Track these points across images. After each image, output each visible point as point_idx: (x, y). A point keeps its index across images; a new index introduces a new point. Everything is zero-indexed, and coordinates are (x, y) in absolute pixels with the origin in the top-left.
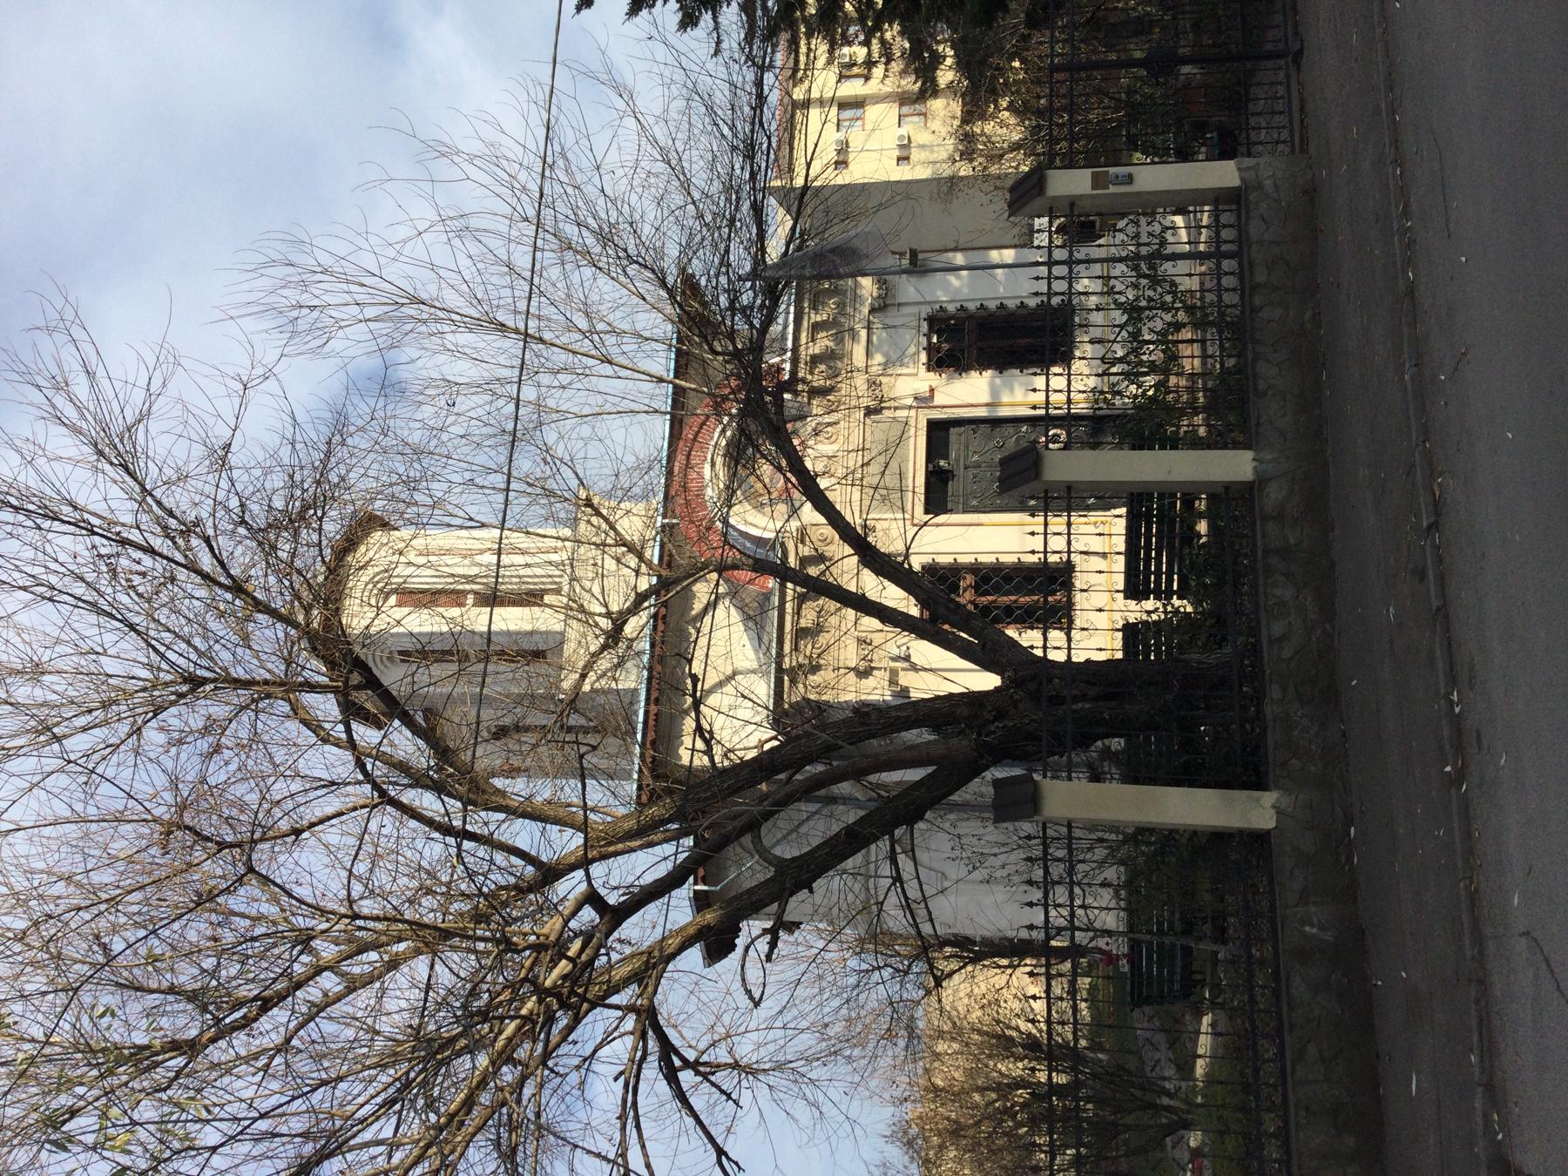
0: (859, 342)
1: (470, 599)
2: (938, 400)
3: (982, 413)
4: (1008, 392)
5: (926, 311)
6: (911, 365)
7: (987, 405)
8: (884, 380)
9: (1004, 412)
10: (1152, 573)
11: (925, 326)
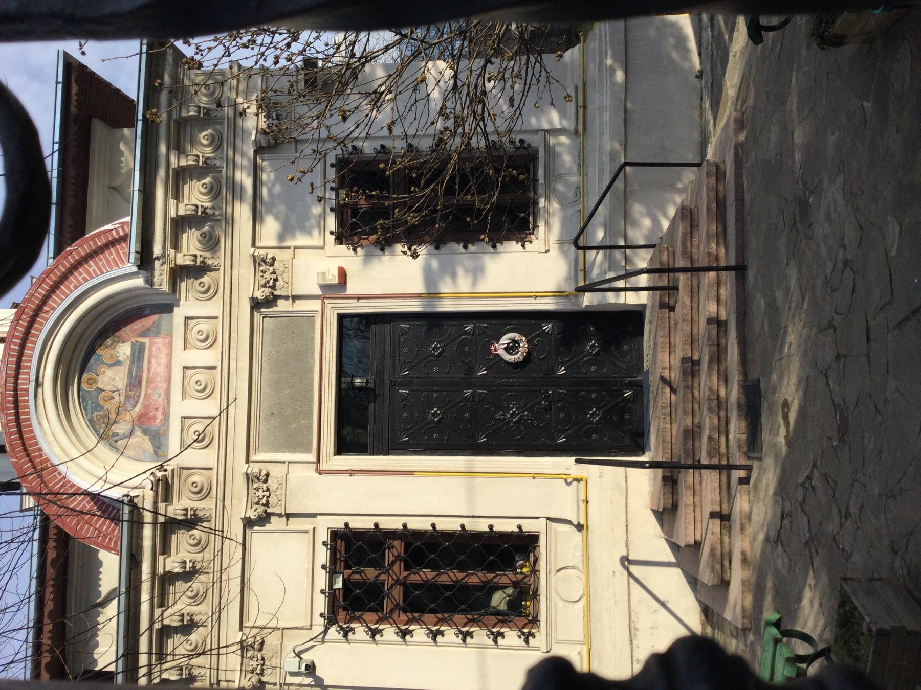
2: (351, 289)
3: (414, 306)
4: (448, 280)
6: (316, 233)
7: (419, 296)
8: (280, 255)
9: (447, 306)
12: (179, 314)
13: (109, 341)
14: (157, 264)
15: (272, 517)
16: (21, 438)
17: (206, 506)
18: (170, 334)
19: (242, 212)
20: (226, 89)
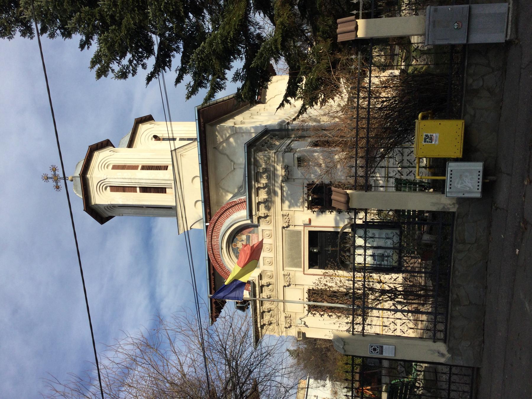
0: (278, 196)
1: (138, 189)
2: (312, 224)
3: (332, 230)
5: (306, 182)
7: (333, 227)
10: (409, 390)
11: (306, 190)
12: (260, 229)
13: (239, 234)
14: (254, 217)
15: (461, 157)
16: (215, 258)
17: (272, 281)
18: (258, 233)
19: (278, 200)
20: (271, 161)
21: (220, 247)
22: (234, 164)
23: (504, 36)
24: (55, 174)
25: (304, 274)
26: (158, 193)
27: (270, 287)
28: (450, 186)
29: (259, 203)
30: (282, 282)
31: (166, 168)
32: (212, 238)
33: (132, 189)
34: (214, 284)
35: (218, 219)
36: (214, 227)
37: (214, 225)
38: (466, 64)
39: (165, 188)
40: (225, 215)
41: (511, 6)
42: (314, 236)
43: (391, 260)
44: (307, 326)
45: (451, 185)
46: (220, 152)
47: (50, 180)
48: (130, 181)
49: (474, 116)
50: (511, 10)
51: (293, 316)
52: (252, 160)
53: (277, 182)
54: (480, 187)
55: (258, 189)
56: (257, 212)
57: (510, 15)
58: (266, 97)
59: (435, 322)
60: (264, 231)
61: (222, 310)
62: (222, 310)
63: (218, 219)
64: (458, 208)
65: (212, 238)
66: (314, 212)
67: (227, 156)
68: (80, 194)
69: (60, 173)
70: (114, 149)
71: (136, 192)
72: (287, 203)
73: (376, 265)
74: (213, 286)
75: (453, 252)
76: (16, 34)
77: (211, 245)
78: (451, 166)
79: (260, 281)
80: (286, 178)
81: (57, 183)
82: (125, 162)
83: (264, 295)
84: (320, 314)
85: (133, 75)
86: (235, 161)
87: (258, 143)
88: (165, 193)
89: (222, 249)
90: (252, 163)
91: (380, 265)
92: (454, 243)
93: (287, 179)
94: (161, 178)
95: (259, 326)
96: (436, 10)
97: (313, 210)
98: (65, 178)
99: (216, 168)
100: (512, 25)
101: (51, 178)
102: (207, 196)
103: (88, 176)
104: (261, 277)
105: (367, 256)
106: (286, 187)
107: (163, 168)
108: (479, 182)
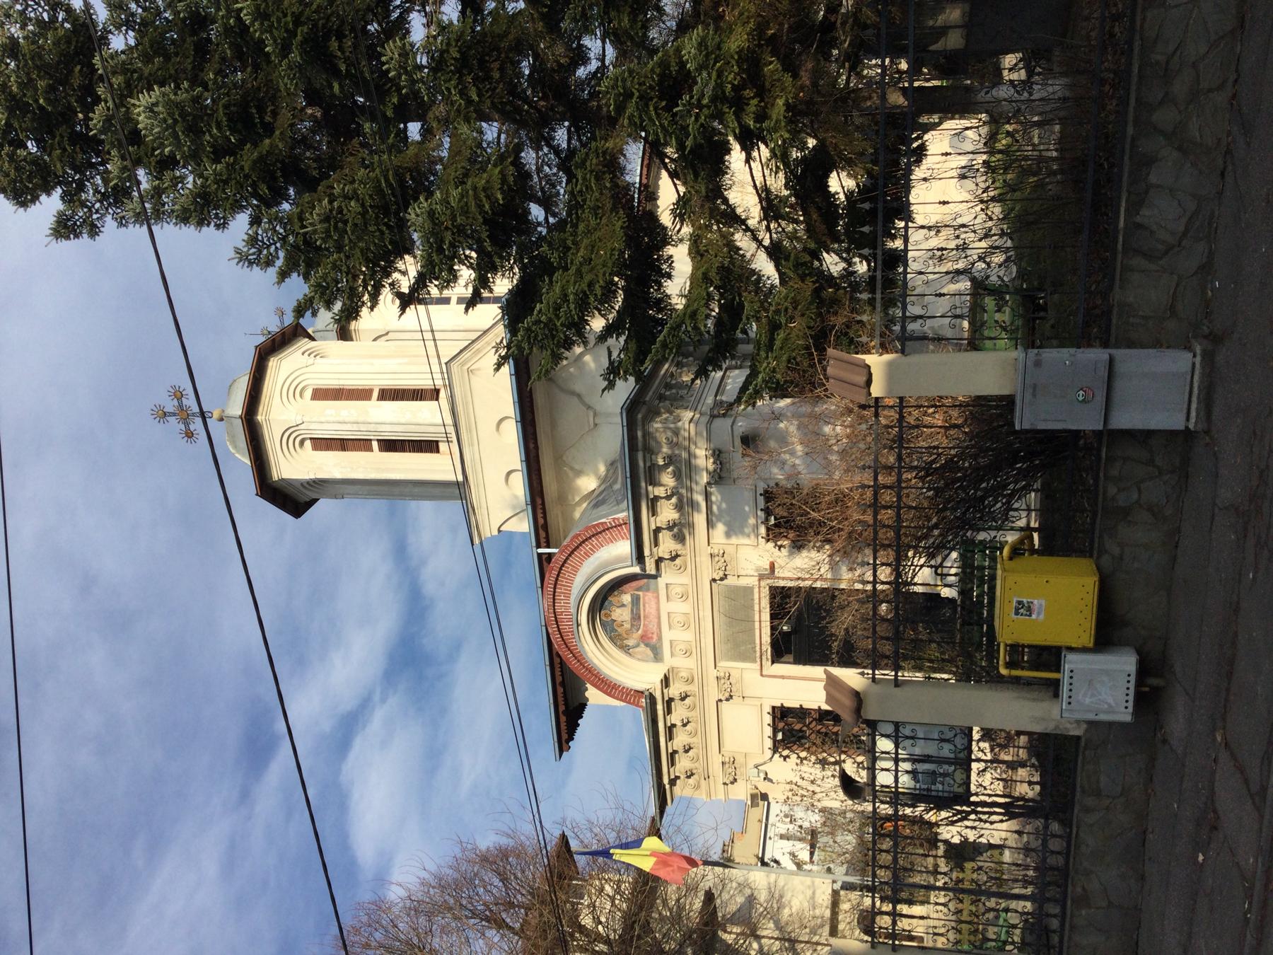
5: (761, 487)
12: (661, 582)
13: (616, 593)
14: (647, 559)
18: (657, 591)
19: (700, 519)
20: (681, 439)
21: (574, 620)
22: (595, 415)
23: (1182, 417)
24: (181, 406)
25: (762, 675)
26: (422, 452)
27: (687, 701)
28: (1070, 694)
29: (657, 531)
30: (713, 693)
31: (434, 394)
32: (554, 599)
33: (362, 444)
34: (562, 675)
35: (567, 558)
36: (558, 575)
37: (559, 572)
38: (1104, 455)
39: (437, 442)
40: (582, 550)
41: (1198, 359)
42: (781, 598)
43: (952, 782)
44: (771, 781)
45: (1070, 697)
46: (563, 390)
47: (172, 419)
48: (355, 427)
49: (1121, 558)
50: (1198, 366)
51: (740, 760)
52: (639, 434)
53: (697, 483)
54: (1130, 704)
55: (657, 531)
56: (655, 550)
57: (1196, 378)
58: (659, 202)
59: (1045, 835)
60: (671, 588)
61: (579, 721)
62: (579, 721)
63: (567, 558)
64: (1086, 731)
65: (554, 599)
66: (780, 547)
67: (579, 396)
68: (243, 455)
69: (190, 402)
70: (313, 344)
71: (371, 450)
72: (720, 528)
73: (920, 789)
74: (559, 679)
75: (1076, 811)
76: (106, 225)
77: (555, 613)
78: (1071, 662)
79: (665, 691)
80: (716, 477)
81: (187, 424)
82: (342, 382)
83: (675, 718)
84: (799, 757)
85: (372, 308)
86: (598, 408)
87: (651, 393)
88: (438, 451)
89: (578, 625)
90: (640, 445)
91: (928, 790)
92: (1078, 794)
93: (719, 477)
94: (426, 422)
95: (666, 781)
96: (1038, 364)
97: (779, 543)
98: (203, 415)
99: (553, 424)
100: (1199, 403)
101: (174, 414)
102: (532, 455)
103: (260, 418)
104: (666, 682)
105: (900, 774)
106: (716, 493)
107: (428, 395)
108: (1127, 695)
